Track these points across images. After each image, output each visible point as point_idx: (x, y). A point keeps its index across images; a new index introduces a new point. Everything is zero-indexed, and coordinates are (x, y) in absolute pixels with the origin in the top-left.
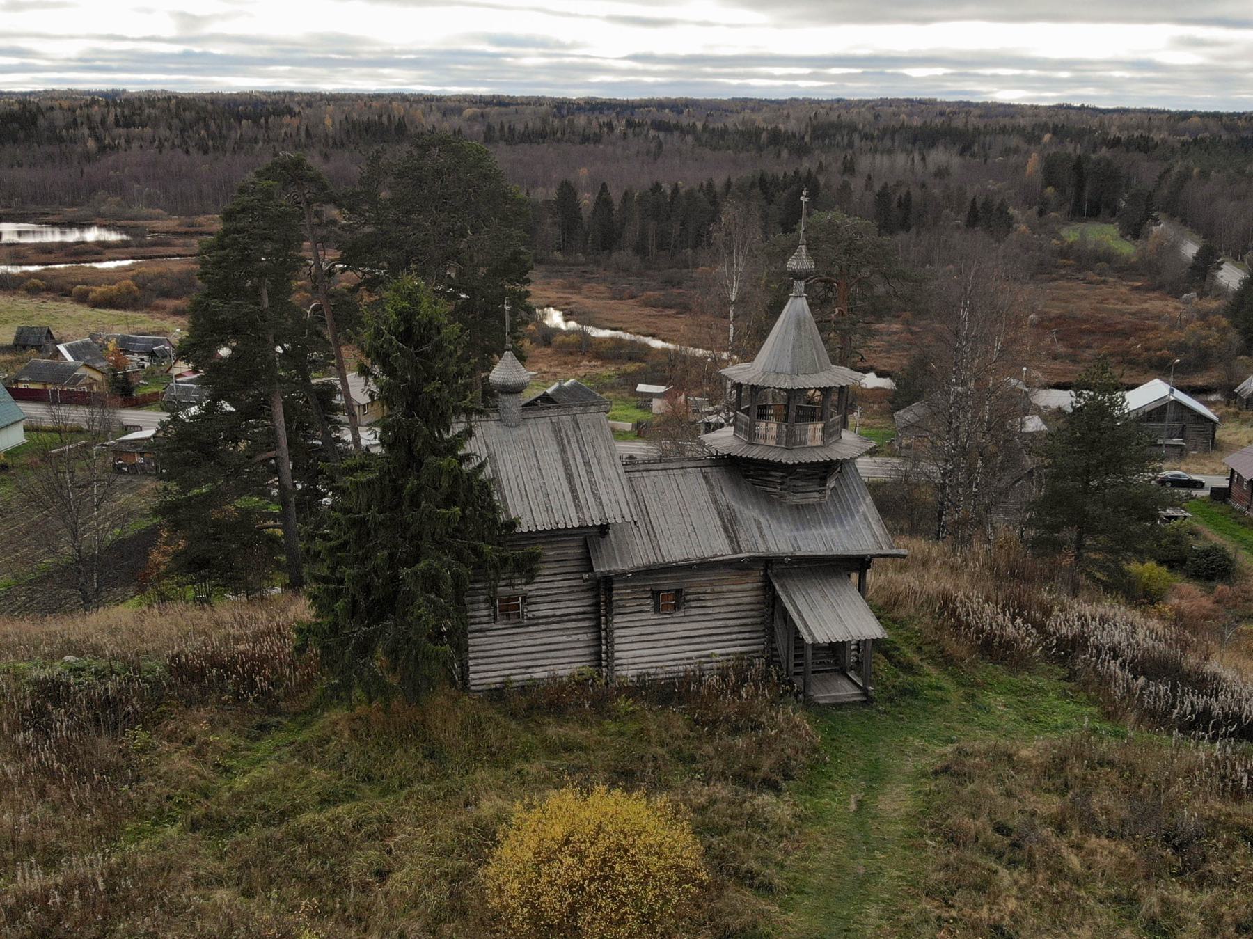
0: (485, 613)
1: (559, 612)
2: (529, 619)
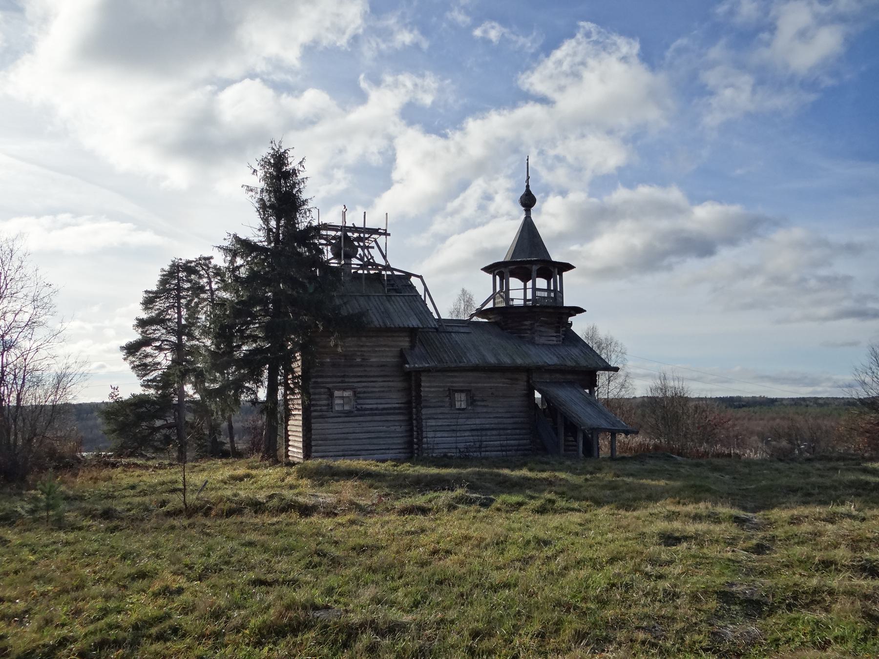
0: (325, 402)
1: (381, 406)
2: (358, 410)
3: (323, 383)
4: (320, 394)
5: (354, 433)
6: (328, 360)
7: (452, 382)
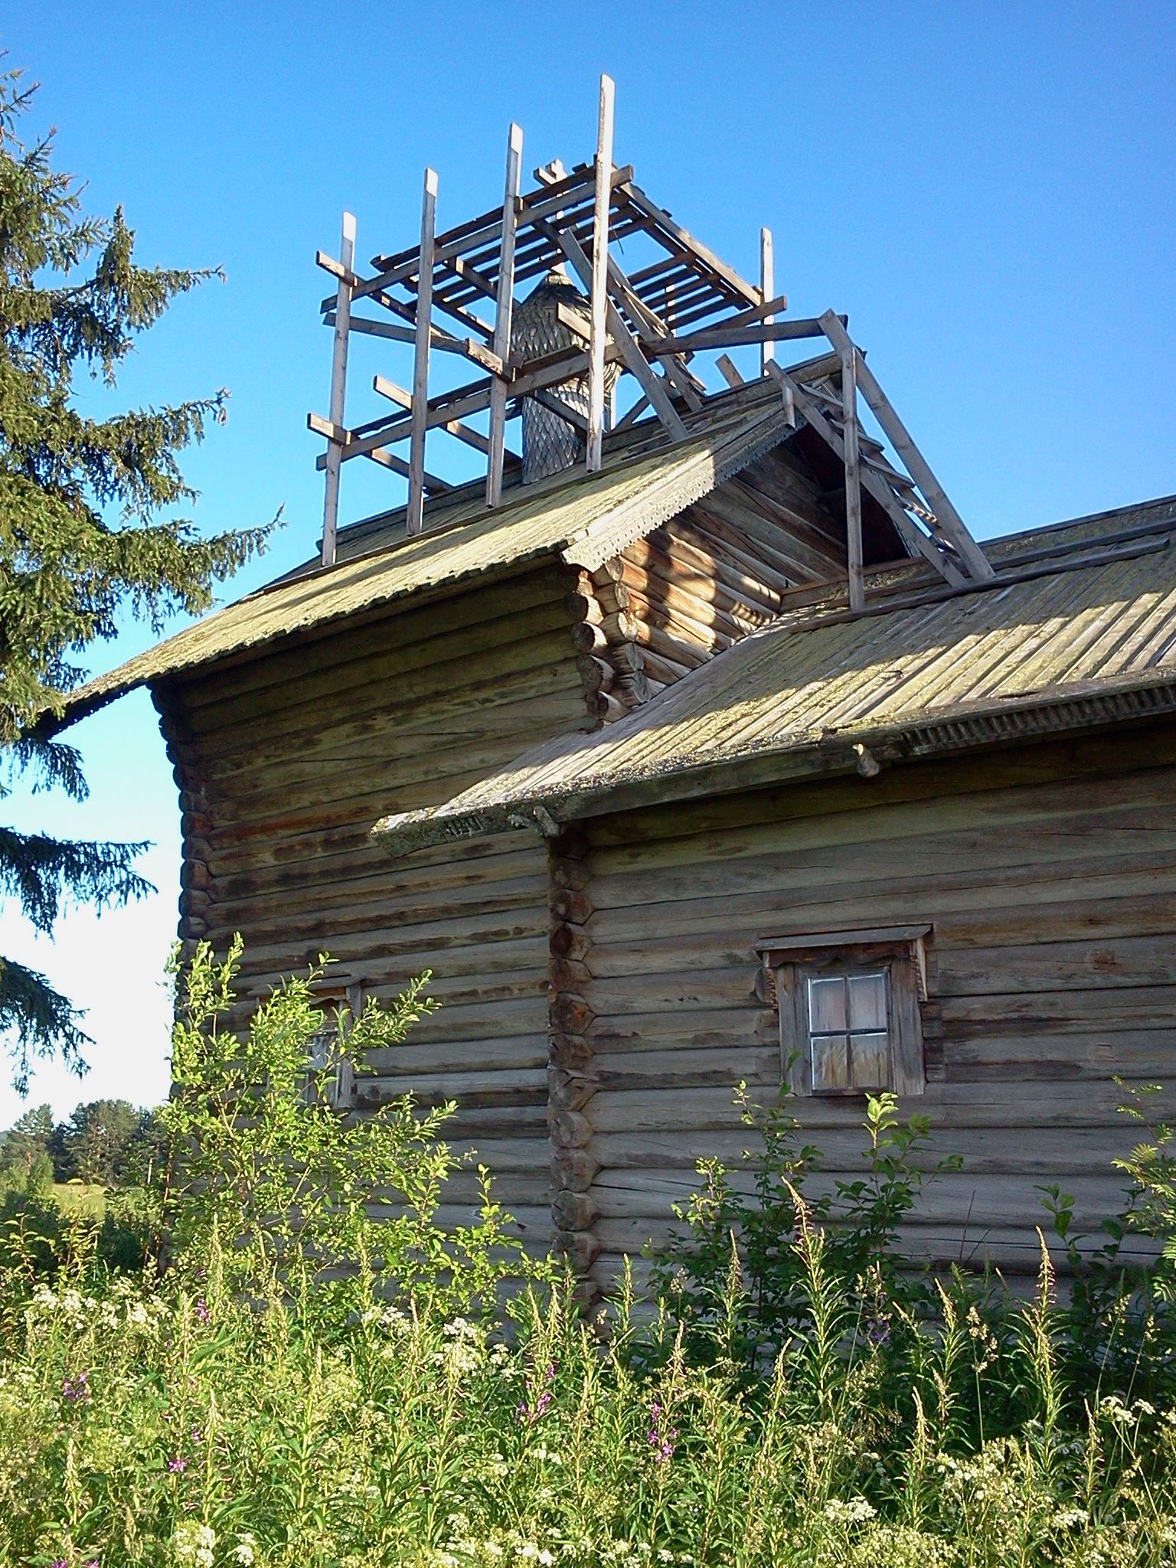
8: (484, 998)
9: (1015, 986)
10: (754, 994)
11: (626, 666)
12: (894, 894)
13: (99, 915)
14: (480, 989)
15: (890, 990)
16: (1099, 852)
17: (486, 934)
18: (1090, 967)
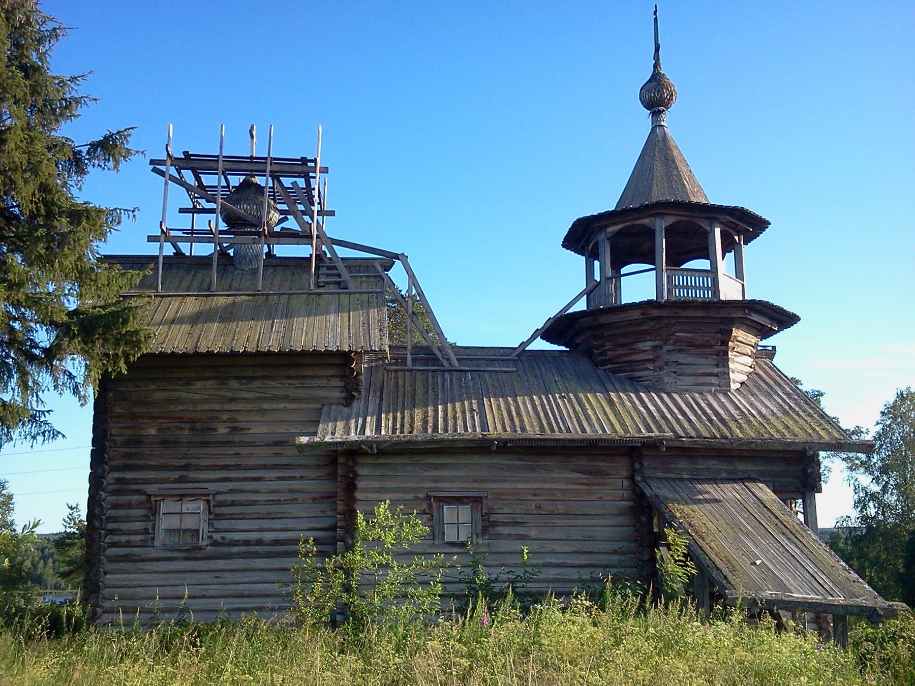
0: (138, 525)
1: (268, 536)
2: (215, 543)
3: (135, 481)
4: (129, 506)
5: (204, 597)
6: (153, 431)
7: (436, 480)
8: (282, 502)
9: (511, 511)
10: (425, 509)
11: (361, 384)
12: (476, 481)
13: (32, 446)
14: (282, 499)
15: (472, 511)
16: (538, 476)
17: (285, 477)
18: (533, 508)
